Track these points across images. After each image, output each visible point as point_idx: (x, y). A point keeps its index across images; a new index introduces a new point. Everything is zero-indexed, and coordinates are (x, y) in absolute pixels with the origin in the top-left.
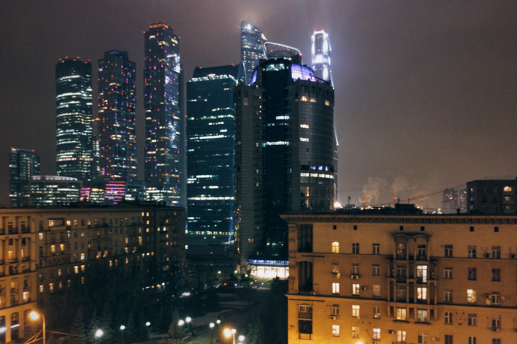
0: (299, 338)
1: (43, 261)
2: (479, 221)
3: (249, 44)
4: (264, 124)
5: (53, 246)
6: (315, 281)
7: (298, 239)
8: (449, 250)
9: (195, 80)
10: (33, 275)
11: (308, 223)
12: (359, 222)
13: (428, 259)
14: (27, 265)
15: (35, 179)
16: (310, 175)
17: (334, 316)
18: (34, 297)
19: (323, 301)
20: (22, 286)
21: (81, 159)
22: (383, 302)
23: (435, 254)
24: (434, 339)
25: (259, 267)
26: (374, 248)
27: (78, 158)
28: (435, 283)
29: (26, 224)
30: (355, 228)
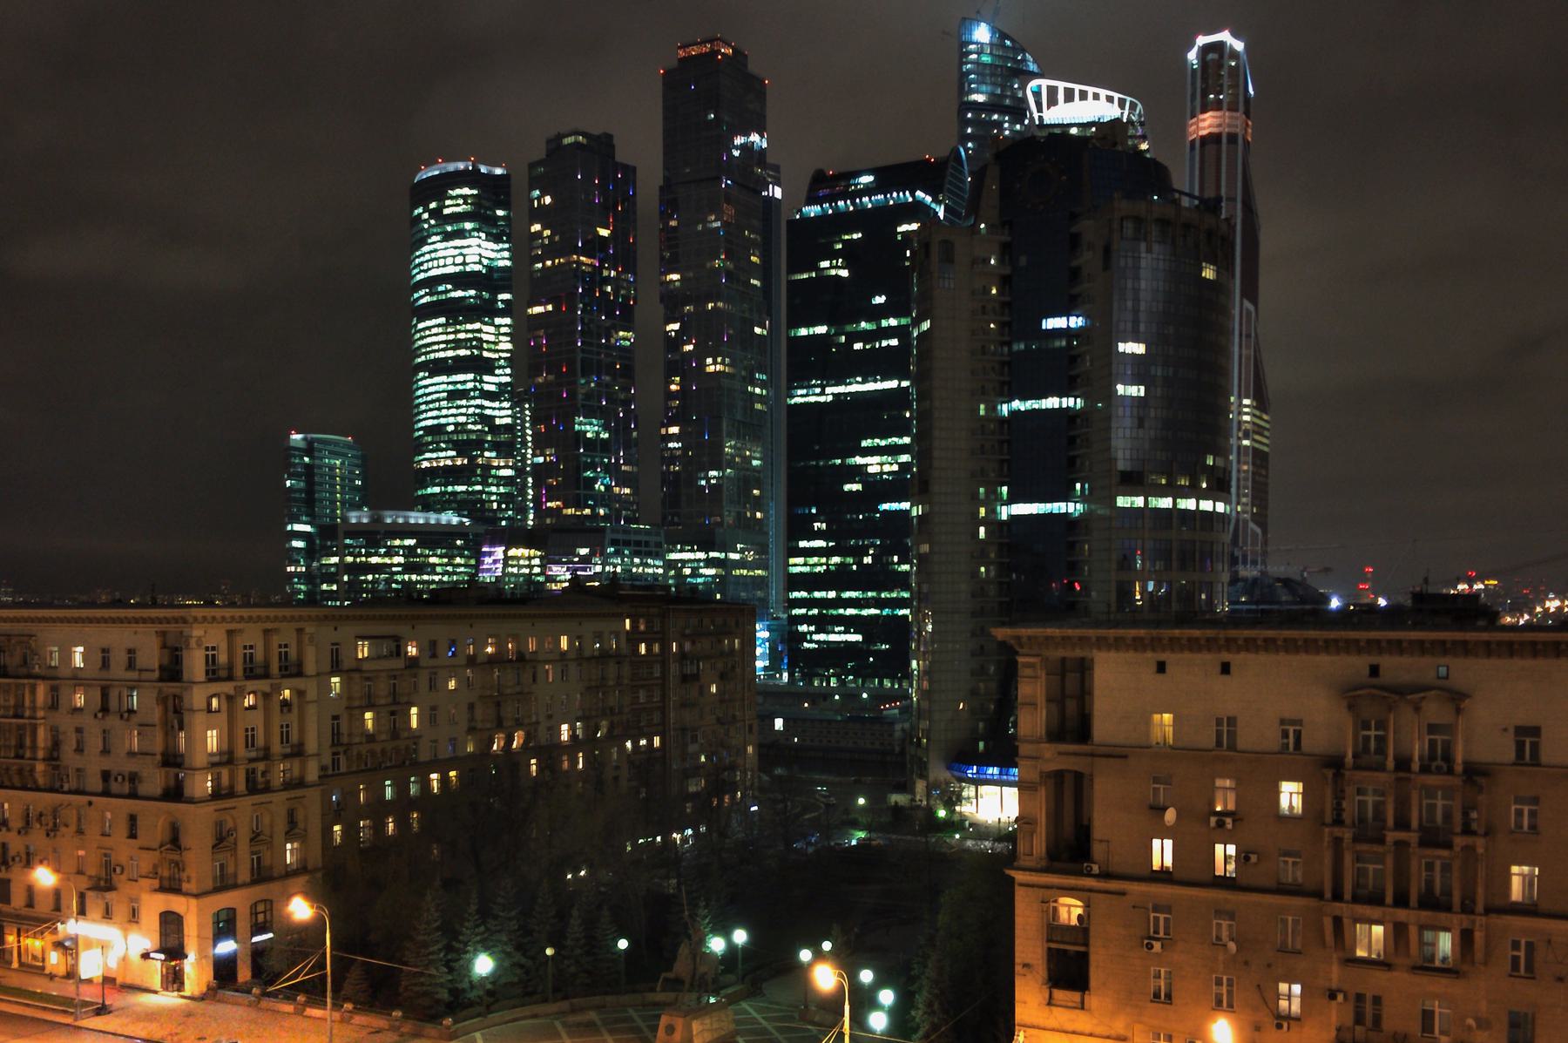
0: (1049, 1004)
1: (342, 758)
2: (1250, 645)
3: (984, 88)
4: (1003, 344)
5: (368, 715)
6: (1099, 831)
7: (1049, 700)
8: (1528, 741)
9: (813, 211)
10: (313, 795)
11: (1078, 653)
12: (1239, 650)
13: (1459, 768)
14: (295, 766)
15: (354, 521)
16: (1146, 502)
17: (1157, 939)
18: (316, 858)
19: (1123, 893)
20: (281, 826)
21: (480, 461)
22: (1312, 902)
23: (1483, 755)
24: (1470, 1021)
25: (983, 789)
26: (1285, 734)
27: (472, 459)
28: (1480, 843)
29: (293, 653)
30: (1226, 669)
